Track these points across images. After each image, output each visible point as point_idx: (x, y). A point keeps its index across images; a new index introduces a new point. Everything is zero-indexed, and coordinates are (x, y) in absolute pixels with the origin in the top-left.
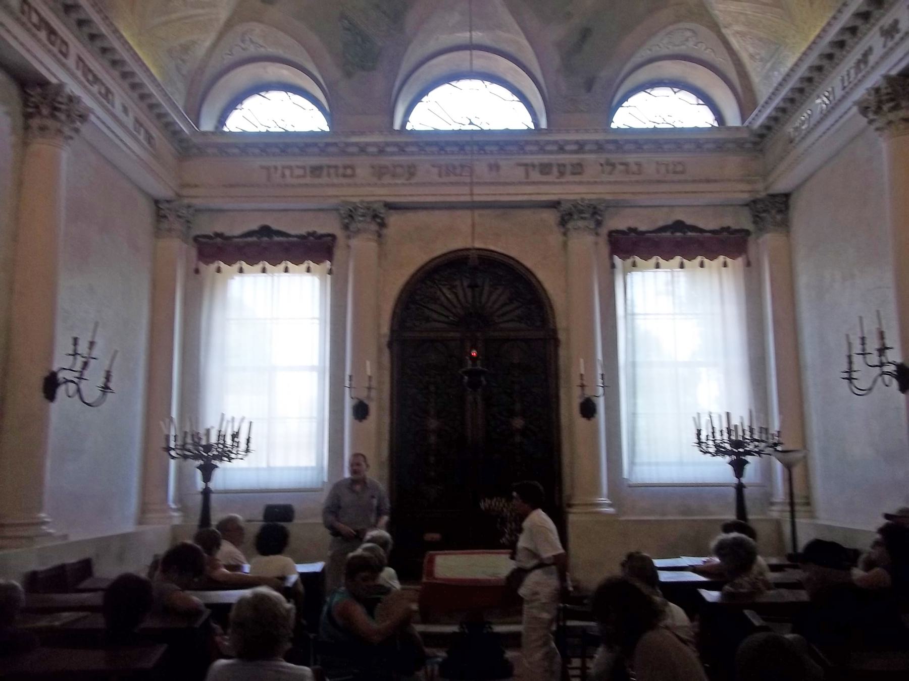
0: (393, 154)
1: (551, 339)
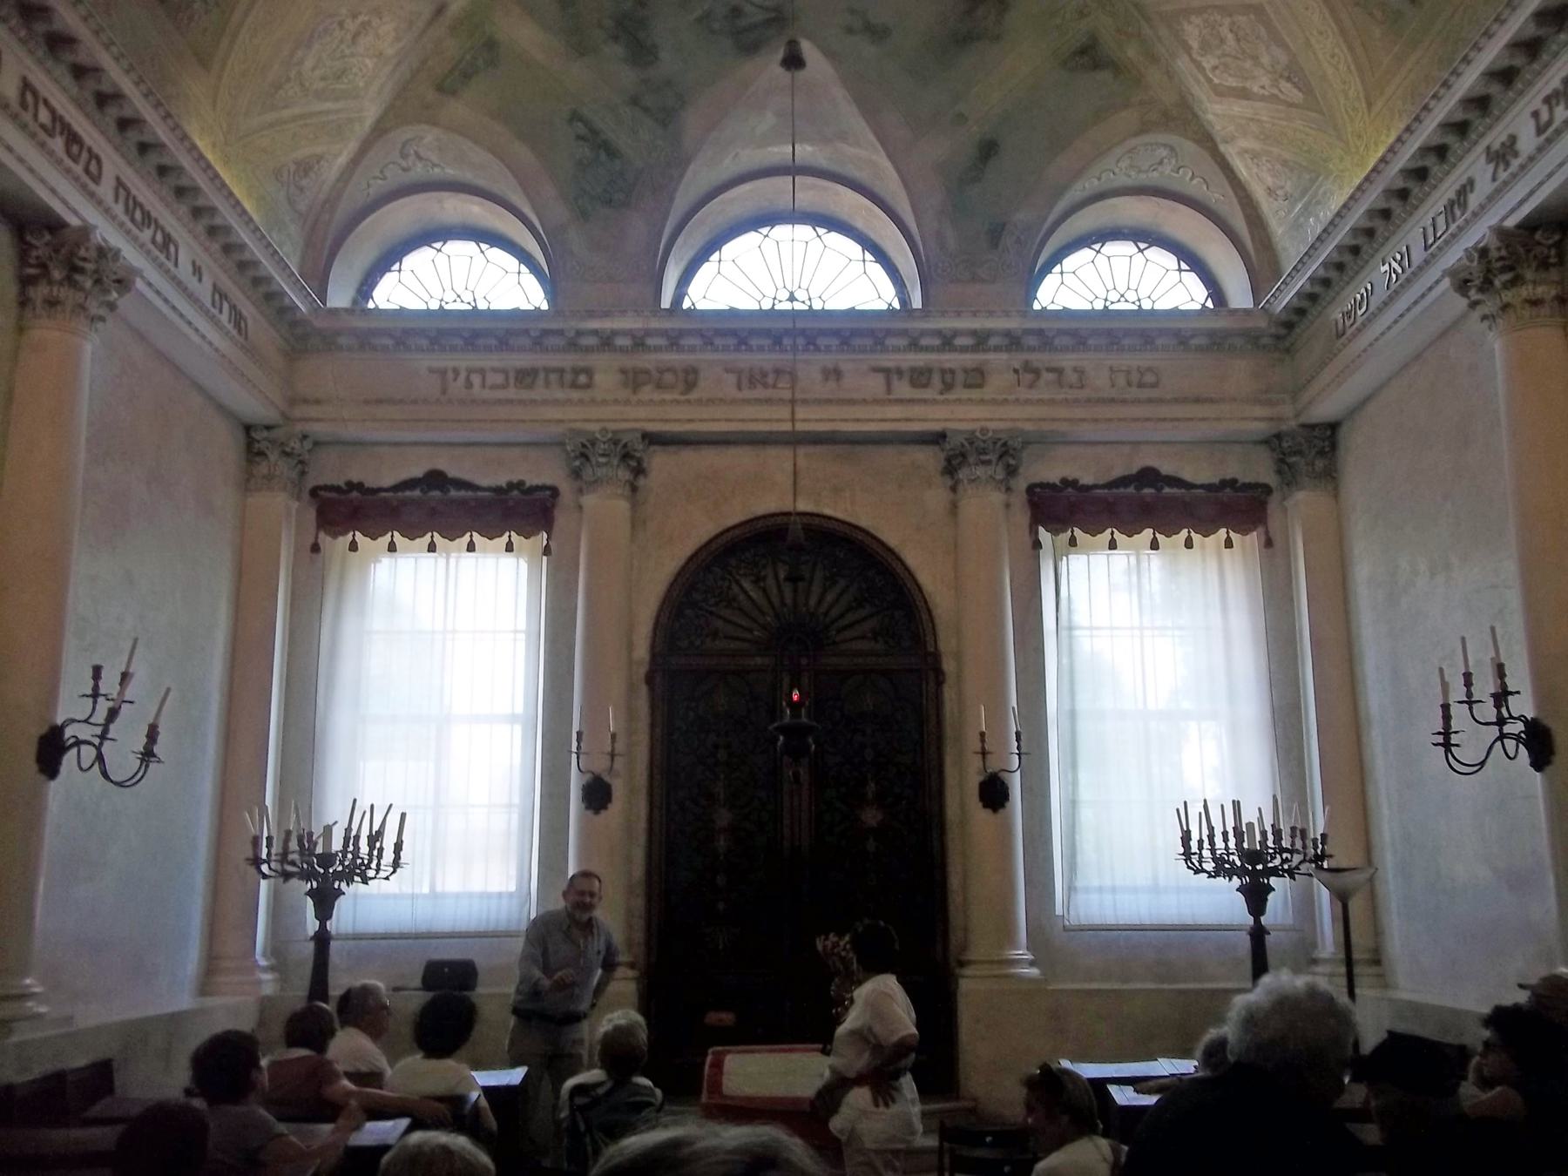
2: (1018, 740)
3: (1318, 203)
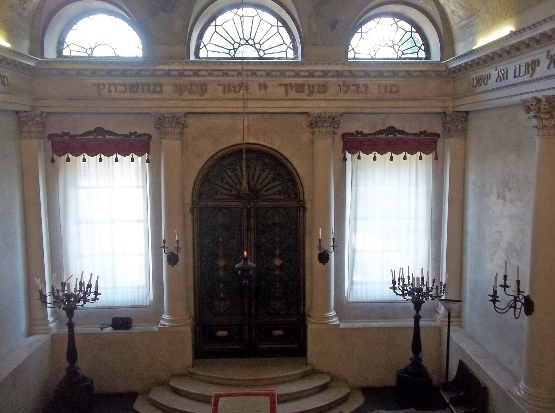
0: (189, 76)
1: (302, 207)
2: (333, 241)
3: (472, 25)
